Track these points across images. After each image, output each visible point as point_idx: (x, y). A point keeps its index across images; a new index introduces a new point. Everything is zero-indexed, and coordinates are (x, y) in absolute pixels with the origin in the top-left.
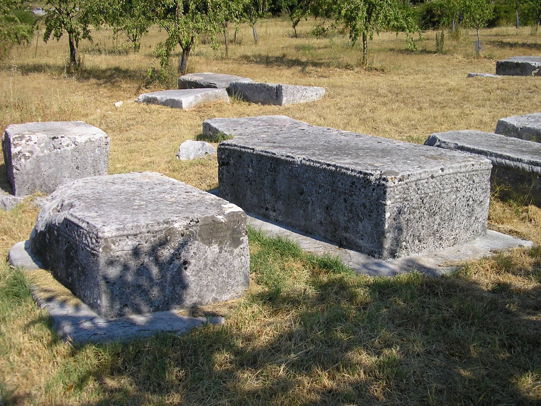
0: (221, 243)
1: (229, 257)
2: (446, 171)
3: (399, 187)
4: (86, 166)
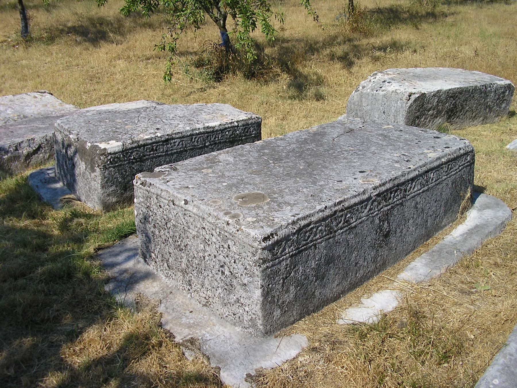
2: (189, 207)
4: (389, 113)
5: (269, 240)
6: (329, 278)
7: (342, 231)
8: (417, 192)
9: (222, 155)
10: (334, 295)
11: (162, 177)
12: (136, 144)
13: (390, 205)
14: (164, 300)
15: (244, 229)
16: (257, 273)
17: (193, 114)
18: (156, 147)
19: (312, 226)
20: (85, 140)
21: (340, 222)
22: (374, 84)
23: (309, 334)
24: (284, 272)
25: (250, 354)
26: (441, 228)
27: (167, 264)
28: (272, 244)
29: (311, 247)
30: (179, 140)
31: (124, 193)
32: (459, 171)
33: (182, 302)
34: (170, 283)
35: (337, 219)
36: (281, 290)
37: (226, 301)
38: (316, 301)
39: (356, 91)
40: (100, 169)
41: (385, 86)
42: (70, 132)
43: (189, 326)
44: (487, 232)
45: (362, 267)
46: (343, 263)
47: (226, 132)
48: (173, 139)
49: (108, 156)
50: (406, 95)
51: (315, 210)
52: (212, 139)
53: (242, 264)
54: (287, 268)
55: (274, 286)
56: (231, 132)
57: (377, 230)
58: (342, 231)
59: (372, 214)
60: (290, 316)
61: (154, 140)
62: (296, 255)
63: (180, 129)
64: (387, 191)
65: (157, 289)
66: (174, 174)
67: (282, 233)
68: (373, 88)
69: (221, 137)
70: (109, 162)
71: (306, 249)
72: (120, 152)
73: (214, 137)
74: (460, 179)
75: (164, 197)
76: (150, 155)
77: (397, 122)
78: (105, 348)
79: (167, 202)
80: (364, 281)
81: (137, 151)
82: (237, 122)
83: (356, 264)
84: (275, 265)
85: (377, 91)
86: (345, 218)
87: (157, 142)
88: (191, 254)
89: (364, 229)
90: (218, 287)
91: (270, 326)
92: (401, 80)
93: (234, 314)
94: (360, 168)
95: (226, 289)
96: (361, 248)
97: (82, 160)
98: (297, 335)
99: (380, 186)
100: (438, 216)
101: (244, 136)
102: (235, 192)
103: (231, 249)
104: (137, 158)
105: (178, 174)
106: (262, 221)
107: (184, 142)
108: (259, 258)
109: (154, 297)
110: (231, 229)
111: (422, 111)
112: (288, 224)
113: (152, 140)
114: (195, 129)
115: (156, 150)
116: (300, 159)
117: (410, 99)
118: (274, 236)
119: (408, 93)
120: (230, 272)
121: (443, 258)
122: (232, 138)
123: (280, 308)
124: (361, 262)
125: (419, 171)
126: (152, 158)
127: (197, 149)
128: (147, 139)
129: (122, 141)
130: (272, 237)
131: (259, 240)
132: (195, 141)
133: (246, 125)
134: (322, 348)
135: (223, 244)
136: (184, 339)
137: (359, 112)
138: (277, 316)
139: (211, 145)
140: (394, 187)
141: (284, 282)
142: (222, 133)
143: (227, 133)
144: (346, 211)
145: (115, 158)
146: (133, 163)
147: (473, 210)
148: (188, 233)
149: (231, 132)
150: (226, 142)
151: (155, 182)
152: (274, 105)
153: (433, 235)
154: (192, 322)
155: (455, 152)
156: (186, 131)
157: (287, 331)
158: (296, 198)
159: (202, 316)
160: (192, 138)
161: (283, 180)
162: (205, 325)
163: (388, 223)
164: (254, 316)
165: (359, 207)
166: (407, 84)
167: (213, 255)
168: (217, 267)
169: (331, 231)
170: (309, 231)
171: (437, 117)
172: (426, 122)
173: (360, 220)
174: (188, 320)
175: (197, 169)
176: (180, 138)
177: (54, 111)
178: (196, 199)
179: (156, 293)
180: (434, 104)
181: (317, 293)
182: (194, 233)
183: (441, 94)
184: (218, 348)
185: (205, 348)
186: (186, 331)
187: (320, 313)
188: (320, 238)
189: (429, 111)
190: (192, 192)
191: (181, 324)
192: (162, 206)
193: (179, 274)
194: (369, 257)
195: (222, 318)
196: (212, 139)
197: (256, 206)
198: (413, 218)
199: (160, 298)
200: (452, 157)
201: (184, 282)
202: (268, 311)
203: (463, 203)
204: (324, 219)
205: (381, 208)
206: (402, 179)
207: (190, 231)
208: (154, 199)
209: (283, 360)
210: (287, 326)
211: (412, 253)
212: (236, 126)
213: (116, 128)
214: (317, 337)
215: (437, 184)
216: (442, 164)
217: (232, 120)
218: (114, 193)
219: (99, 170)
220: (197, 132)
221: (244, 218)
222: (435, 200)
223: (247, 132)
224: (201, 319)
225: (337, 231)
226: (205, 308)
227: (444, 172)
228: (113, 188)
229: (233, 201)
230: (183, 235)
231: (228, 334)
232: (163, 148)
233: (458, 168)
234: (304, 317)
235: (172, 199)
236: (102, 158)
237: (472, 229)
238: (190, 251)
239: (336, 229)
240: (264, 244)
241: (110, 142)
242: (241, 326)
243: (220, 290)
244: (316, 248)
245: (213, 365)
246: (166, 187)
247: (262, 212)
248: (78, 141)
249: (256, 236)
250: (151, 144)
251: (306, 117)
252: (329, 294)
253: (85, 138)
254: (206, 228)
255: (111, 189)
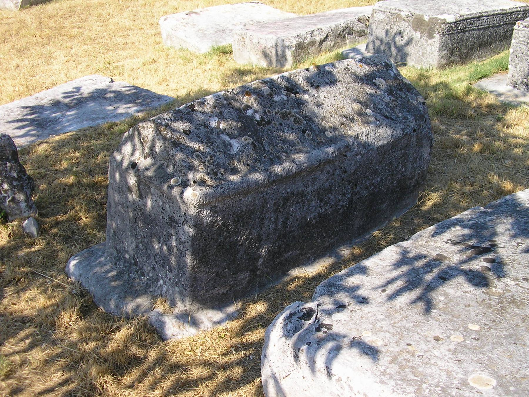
0: (422, 33)
1: (425, 43)
3: (523, 32)
30: (486, 18)
48: (483, 16)
52: (505, 20)
56: (516, 15)
146: (459, 33)
149: (516, 15)
236: (442, 26)
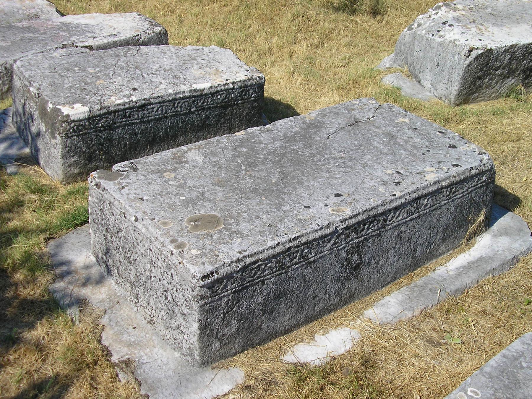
2: (139, 225)
4: (444, 68)
5: (208, 279)
6: (279, 311)
7: (296, 266)
8: (402, 221)
9: (193, 151)
10: (285, 328)
11: (119, 180)
12: (105, 111)
13: (362, 236)
14: (109, 311)
15: (185, 263)
16: (195, 307)
17: (182, 66)
18: (130, 113)
19: (260, 263)
20: (46, 98)
21: (295, 258)
22: (432, 24)
23: (247, 369)
24: (225, 307)
25: (182, 384)
26: (437, 256)
27: (118, 271)
28: (211, 282)
29: (257, 283)
31: (88, 164)
32: (468, 194)
33: (127, 315)
34: (120, 291)
35: (290, 255)
36: (221, 324)
37: (168, 324)
38: (262, 334)
39: (408, 30)
40: (62, 137)
41: (444, 31)
42: (30, 83)
43: (129, 345)
44: (489, 268)
45: (322, 300)
46: (297, 297)
47: (217, 96)
48: (151, 104)
49: (71, 124)
50: (465, 49)
51: (265, 247)
53: (183, 295)
54: (228, 303)
55: (213, 320)
56: (224, 96)
57: (343, 263)
58: (296, 266)
59: (337, 247)
60: (231, 348)
61: (127, 106)
62: (239, 291)
63: (161, 91)
64: (359, 223)
65: (104, 296)
66: (133, 176)
67: (223, 272)
68: (429, 30)
69: (211, 102)
70: (71, 130)
71: (252, 285)
72: (86, 119)
73: (202, 101)
74: (469, 202)
75: (117, 206)
76: (122, 122)
77: (451, 81)
78: (40, 360)
79: (119, 212)
80: (324, 315)
81: (107, 118)
82: (232, 83)
83: (314, 298)
84: (215, 302)
85: (433, 35)
86: (302, 253)
87: (131, 108)
88: (139, 270)
89: (326, 263)
90: (162, 309)
91: (208, 358)
92: (468, 22)
93: (175, 339)
94: (339, 188)
95: (168, 314)
96: (321, 282)
97: (42, 121)
98: (236, 369)
99: (350, 218)
100: (432, 244)
101: (241, 100)
102: (190, 211)
103: (174, 278)
104: (106, 126)
105: (137, 176)
106: (206, 256)
107: (164, 108)
108: (197, 295)
109: (99, 306)
110: (174, 260)
111: (485, 71)
112: (232, 262)
113: (125, 105)
114: (179, 93)
115: (130, 117)
116: (277, 167)
117: (470, 55)
118: (215, 274)
119: (468, 47)
120: (172, 298)
121: (423, 296)
122: (225, 102)
123: (219, 340)
124: (321, 296)
125: (406, 199)
126: (125, 126)
127: (180, 115)
128: (119, 105)
129: (89, 105)
130: (212, 275)
131: (197, 278)
132: (177, 107)
133: (244, 87)
134: (257, 387)
135: (167, 270)
136: (121, 359)
137: (409, 57)
138: (216, 348)
139: (198, 110)
140: (369, 218)
141: (224, 317)
142: (212, 96)
143: (219, 97)
144: (302, 247)
145: (79, 125)
146: (101, 131)
147: (487, 235)
148: (136, 249)
150: (216, 107)
151: (109, 187)
152: (312, 19)
153: (424, 264)
154: (133, 340)
155: (463, 173)
156: (167, 95)
157: (226, 362)
158: (252, 226)
159: (145, 334)
160: (175, 103)
161: (246, 199)
162: (145, 345)
163: (360, 255)
164: (192, 346)
165: (321, 242)
166: (474, 30)
167: (158, 277)
168: (161, 290)
169: (282, 267)
170: (256, 268)
171: (508, 77)
172: (491, 83)
173: (321, 254)
174: (129, 338)
175: (159, 171)
176: (160, 103)
177: (21, 9)
178: (147, 217)
179: (103, 301)
180: (505, 62)
181: (264, 326)
182: (142, 251)
183: (516, 49)
184: (152, 374)
185: (139, 372)
186: (125, 350)
187: (266, 346)
188: (270, 274)
189: (496, 70)
190: (145, 206)
191: (121, 341)
192: (114, 214)
193: (128, 285)
194: (332, 290)
195: (163, 339)
196: (200, 104)
197: (206, 233)
198: (395, 248)
199: (106, 307)
200: (458, 179)
201: (132, 294)
202: (205, 343)
203: (471, 229)
204: (274, 256)
205: (350, 241)
206: (381, 209)
207: (139, 247)
208: (107, 204)
209: (213, 394)
210: (226, 358)
211: (390, 285)
212: (230, 89)
213: (85, 84)
214: (256, 373)
215: (433, 210)
216: (442, 188)
217: (227, 80)
218: (77, 163)
219: (60, 138)
220: (181, 96)
221: (189, 249)
222: (428, 227)
223: (245, 95)
224: (143, 337)
225: (291, 266)
226: (149, 325)
227: (444, 196)
228: (76, 158)
229: (185, 223)
230: (132, 249)
231: (166, 359)
232: (138, 115)
233: (467, 190)
234: (247, 349)
235: (123, 211)
236: (64, 125)
237: (473, 262)
238: (138, 266)
239: (289, 264)
240: (202, 283)
241: (75, 106)
242: (180, 352)
243: (163, 313)
244: (263, 284)
245: (143, 392)
246: (120, 195)
247: (210, 242)
248: (39, 97)
249: (195, 274)
250: (123, 110)
251: (348, 45)
252: (279, 327)
253: (46, 95)
254: (153, 250)
255: (73, 160)
